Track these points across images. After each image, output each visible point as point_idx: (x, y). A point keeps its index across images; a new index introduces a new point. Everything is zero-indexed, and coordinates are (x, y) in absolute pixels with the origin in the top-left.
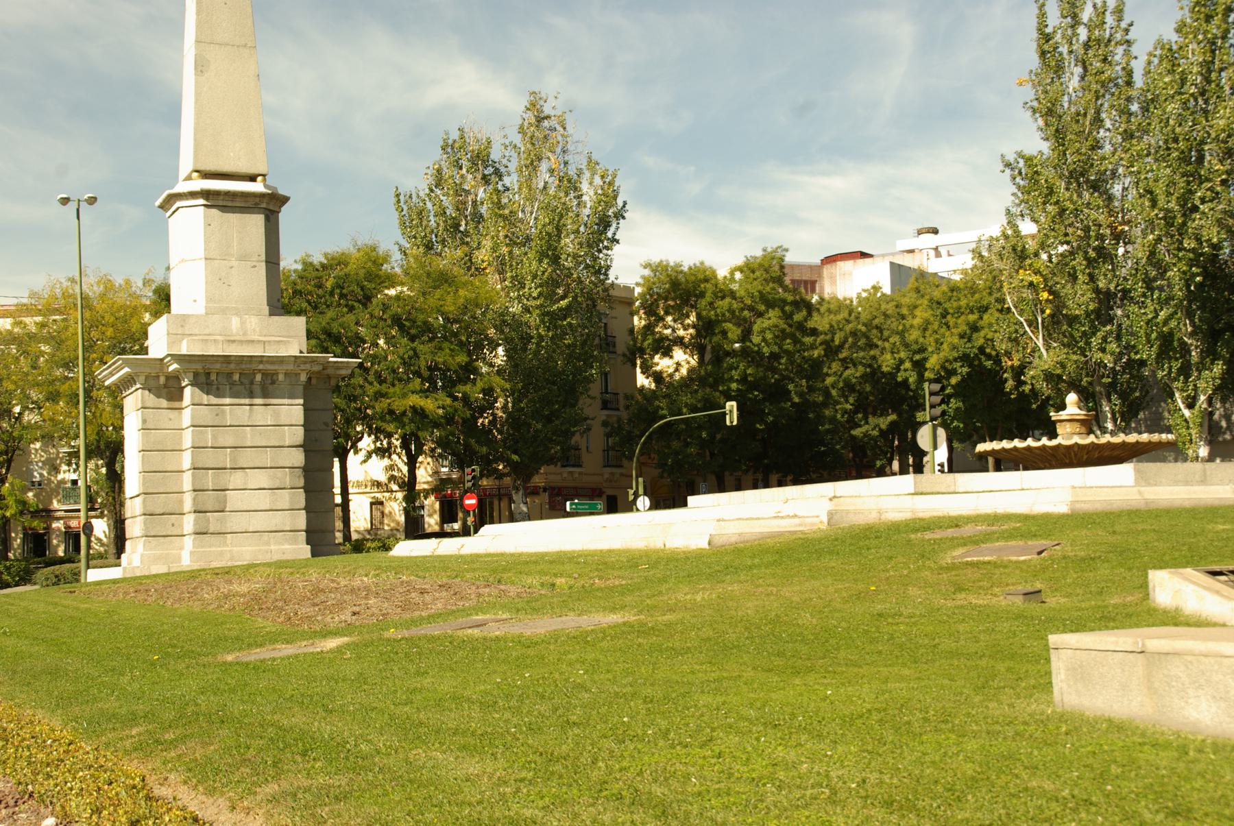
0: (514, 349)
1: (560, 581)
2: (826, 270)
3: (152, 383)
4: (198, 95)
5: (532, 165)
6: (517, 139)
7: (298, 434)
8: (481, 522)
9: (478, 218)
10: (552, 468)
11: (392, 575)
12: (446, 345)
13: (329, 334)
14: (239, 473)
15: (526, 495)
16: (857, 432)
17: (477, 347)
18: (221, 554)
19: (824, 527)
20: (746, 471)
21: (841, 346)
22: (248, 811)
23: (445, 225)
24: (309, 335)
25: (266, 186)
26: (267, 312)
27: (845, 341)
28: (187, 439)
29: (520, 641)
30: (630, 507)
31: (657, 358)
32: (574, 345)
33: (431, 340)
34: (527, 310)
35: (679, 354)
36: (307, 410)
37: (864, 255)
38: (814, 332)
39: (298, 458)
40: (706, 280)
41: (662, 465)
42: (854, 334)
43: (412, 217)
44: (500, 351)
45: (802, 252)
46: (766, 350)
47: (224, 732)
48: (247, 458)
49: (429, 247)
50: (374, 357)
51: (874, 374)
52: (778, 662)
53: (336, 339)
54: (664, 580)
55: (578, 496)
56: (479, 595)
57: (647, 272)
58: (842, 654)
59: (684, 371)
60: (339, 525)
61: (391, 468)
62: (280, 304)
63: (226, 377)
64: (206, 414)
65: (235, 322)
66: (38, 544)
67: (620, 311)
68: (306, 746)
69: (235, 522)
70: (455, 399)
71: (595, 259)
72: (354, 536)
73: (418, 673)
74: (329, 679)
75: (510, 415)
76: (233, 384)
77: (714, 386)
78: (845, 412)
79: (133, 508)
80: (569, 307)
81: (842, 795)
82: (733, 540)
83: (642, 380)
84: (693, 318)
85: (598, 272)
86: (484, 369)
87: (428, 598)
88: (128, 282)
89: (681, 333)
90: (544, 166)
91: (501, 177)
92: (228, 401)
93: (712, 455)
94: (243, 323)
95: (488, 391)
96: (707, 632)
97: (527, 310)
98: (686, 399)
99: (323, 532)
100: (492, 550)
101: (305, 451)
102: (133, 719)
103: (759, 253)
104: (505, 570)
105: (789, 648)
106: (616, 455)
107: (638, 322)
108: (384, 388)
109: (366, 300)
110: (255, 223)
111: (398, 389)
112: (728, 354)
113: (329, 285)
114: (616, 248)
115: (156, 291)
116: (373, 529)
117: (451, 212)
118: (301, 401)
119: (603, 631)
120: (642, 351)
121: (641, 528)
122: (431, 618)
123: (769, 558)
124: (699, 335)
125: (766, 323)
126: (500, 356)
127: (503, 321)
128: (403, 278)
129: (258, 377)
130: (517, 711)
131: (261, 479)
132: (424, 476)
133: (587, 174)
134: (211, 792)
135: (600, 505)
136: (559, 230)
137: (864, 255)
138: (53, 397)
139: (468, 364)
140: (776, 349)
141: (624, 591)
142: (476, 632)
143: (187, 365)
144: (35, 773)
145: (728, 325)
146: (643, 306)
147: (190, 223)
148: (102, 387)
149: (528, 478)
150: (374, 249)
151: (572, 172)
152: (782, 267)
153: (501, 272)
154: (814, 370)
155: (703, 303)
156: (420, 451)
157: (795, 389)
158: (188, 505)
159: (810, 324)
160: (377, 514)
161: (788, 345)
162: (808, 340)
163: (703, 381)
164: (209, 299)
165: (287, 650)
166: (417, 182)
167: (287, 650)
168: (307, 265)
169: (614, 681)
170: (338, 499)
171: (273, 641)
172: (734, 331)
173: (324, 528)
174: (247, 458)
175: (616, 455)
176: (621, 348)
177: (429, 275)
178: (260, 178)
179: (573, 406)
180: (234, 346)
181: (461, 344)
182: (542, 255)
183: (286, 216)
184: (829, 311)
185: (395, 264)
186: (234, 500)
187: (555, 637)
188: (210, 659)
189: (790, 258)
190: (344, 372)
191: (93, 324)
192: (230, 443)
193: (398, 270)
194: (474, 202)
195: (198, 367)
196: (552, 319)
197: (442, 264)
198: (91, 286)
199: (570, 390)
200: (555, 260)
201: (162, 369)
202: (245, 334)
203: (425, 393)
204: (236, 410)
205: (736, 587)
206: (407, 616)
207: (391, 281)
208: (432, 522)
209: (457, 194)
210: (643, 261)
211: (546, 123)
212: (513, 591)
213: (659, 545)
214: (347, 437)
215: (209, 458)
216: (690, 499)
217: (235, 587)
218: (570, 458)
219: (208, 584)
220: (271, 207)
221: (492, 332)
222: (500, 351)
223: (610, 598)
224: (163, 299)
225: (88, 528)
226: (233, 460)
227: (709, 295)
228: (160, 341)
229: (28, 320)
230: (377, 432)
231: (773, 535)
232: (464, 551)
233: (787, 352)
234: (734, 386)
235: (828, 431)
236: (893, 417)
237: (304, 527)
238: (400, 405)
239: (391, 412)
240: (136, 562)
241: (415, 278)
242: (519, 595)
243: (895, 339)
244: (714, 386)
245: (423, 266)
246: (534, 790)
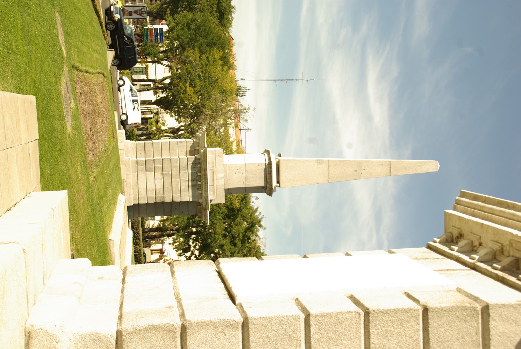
3: (196, 145)
7: (177, 199)
14: (161, 177)
25: (276, 187)
26: (226, 188)
36: (188, 202)
39: (168, 200)
64: (184, 163)
65: (222, 175)
69: (142, 176)
76: (196, 173)
82: (112, 249)
92: (190, 171)
94: (221, 178)
99: (139, 213)
101: (171, 202)
110: (261, 183)
118: (191, 200)
129: (199, 183)
131: (159, 185)
143: (203, 155)
174: (167, 179)
178: (278, 185)
180: (212, 174)
186: (151, 175)
192: (173, 173)
195: (202, 159)
201: (201, 147)
202: (217, 179)
204: (186, 175)
215: (167, 165)
220: (267, 189)
237: (140, 203)
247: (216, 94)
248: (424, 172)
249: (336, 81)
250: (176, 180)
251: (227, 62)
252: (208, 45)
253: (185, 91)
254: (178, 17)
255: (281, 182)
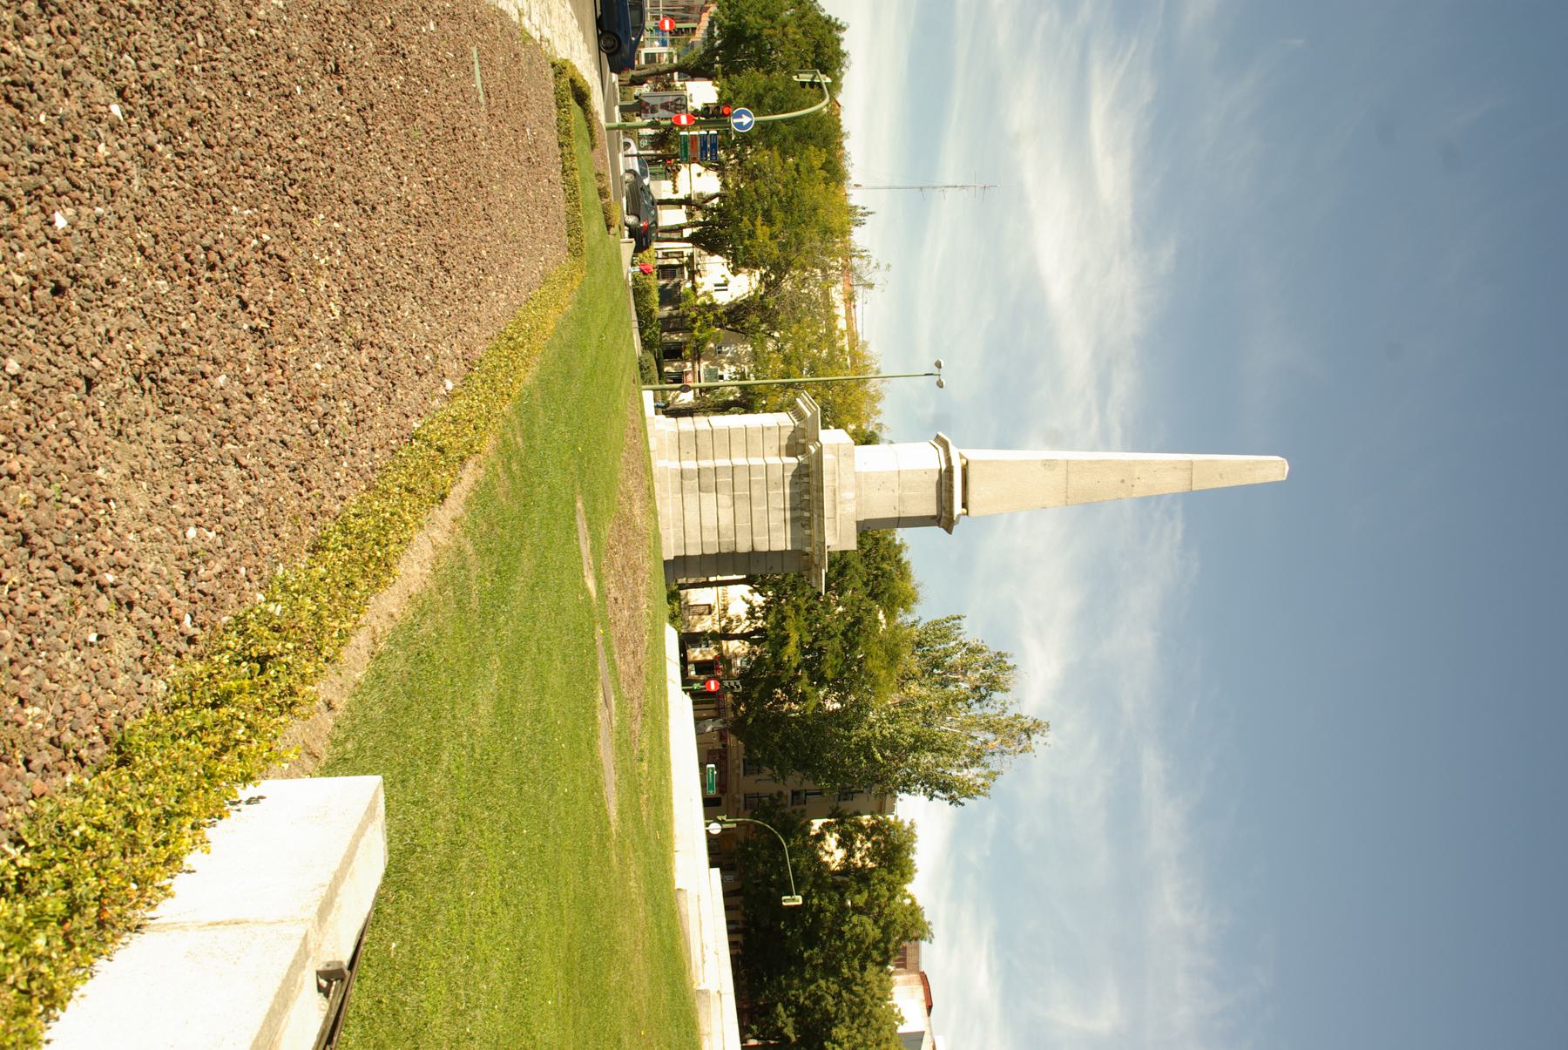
0: (838, 717)
1: (645, 765)
2: (915, 977)
3: (799, 433)
4: (1027, 462)
5: (989, 726)
6: (1010, 713)
8: (695, 695)
9: (944, 684)
10: (742, 751)
11: (649, 627)
12: (840, 661)
13: (845, 567)
15: (720, 731)
16: (780, 1008)
17: (840, 686)
18: (666, 490)
19: (695, 987)
20: (744, 914)
21: (851, 992)
22: (452, 532)
23: (935, 657)
24: (843, 553)
27: (856, 995)
28: (756, 461)
29: (593, 736)
30: (710, 816)
31: (836, 835)
32: (844, 765)
33: (844, 649)
34: (871, 726)
35: (840, 854)
37: (929, 1008)
38: (863, 968)
39: (744, 547)
40: (902, 875)
41: (747, 843)
42: (863, 1002)
43: (942, 630)
44: (837, 706)
45: (931, 954)
46: (845, 928)
47: (516, 508)
48: (742, 507)
49: (919, 645)
50: (828, 604)
51: (829, 1021)
52: (577, 956)
53: (841, 573)
54: (647, 853)
55: (720, 774)
56: (632, 700)
57: (907, 825)
58: (585, 1010)
59: (826, 858)
60: (691, 581)
61: (739, 620)
62: (866, 530)
63: (806, 491)
64: (776, 475)
65: (849, 494)
66: (674, 353)
67: (874, 803)
68: (503, 574)
69: (691, 500)
70: (796, 670)
71: (916, 781)
72: (683, 592)
73: (565, 656)
74: (560, 586)
75: (785, 715)
76: (801, 495)
77: (814, 885)
78: (797, 997)
79: (701, 422)
80: (876, 761)
81: (460, 1021)
83: (817, 824)
84: (870, 865)
85: (905, 784)
86: (821, 693)
87: (629, 658)
88: (879, 412)
89: (858, 855)
90: (990, 736)
91: (978, 701)
92: (788, 491)
93: (757, 885)
95: (803, 697)
96: (602, 893)
97: (871, 726)
98: (803, 861)
100: (671, 707)
102: (529, 436)
103: (927, 918)
104: (654, 718)
105: (589, 964)
106: (754, 804)
107: (865, 819)
108: (803, 612)
109: (874, 596)
110: (931, 509)
111: (803, 623)
112: (842, 895)
113: (884, 566)
114: (926, 799)
115: (873, 434)
116: (689, 607)
117: (948, 661)
119: (602, 805)
120: (841, 823)
121: (690, 827)
122: (612, 662)
123: (667, 941)
124: (857, 870)
125: (869, 927)
126: (833, 705)
127: (861, 707)
128: (893, 624)
129: (807, 514)
130: (532, 740)
131: (726, 518)
132: (734, 647)
133: (984, 772)
134: (468, 502)
135: (712, 792)
136: (939, 750)
137: (929, 1008)
138: (787, 360)
139: (825, 680)
140: (848, 936)
141: (637, 820)
142: (600, 699)
144: (487, 372)
145: (866, 894)
146: (879, 822)
147: (928, 460)
148: (796, 395)
149: (733, 731)
150: (915, 600)
151: (986, 759)
152: (916, 939)
153: (901, 704)
154: (831, 970)
155: (884, 872)
156: (753, 642)
157: (814, 954)
158: (704, 463)
159: (869, 965)
160: (701, 609)
161: (851, 946)
162: (856, 963)
163: (818, 875)
164: (867, 475)
165: (585, 549)
166: (971, 633)
167: (585, 549)
168: (900, 548)
169: (558, 818)
170: (712, 579)
171: (593, 538)
172: (861, 900)
173: (685, 571)
174: (742, 507)
175: (754, 804)
176: (843, 805)
177: (897, 645)
179: (794, 766)
181: (841, 673)
182: (917, 737)
183: (937, 531)
184: (881, 981)
185: (904, 618)
186: (709, 499)
187: (597, 765)
188: (578, 490)
189: (923, 944)
190: (814, 581)
191: (845, 388)
193: (899, 620)
194: (957, 680)
195: (813, 468)
196: (865, 748)
197: (906, 656)
198: (873, 386)
199: (807, 763)
200: (913, 748)
203: (800, 645)
204: (780, 498)
205: (642, 915)
206: (614, 643)
207: (890, 615)
208: (696, 654)
209: (963, 666)
210: (917, 821)
211: (1024, 736)
212: (636, 727)
213: (677, 847)
214: (763, 584)
215: (741, 479)
216: (717, 870)
217: (638, 504)
218: (751, 766)
219: (641, 483)
221: (852, 698)
222: (837, 706)
223: (630, 809)
224: (867, 439)
225: (686, 389)
226: (741, 497)
227: (891, 877)
228: (832, 439)
229: (846, 340)
230: (767, 608)
231: (687, 942)
232: (670, 685)
233: (845, 946)
234: (815, 901)
235: (780, 983)
236: (794, 1039)
238: (790, 625)
239: (784, 618)
240: (658, 427)
241: (894, 635)
242: (633, 732)
243: (859, 1039)
244: (814, 885)
245: (903, 640)
246: (464, 761)
247: (812, 237)
248: (1259, 480)
249: (1027, 107)
250: (759, 509)
251: (834, 172)
252: (797, 139)
253: (752, 235)
254: (739, 81)
255: (970, 505)
